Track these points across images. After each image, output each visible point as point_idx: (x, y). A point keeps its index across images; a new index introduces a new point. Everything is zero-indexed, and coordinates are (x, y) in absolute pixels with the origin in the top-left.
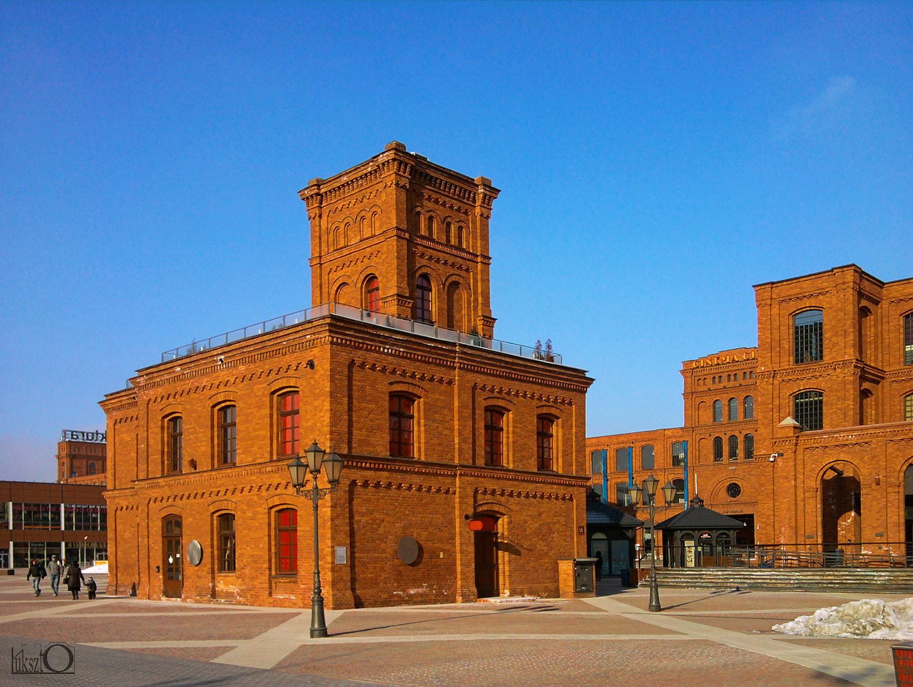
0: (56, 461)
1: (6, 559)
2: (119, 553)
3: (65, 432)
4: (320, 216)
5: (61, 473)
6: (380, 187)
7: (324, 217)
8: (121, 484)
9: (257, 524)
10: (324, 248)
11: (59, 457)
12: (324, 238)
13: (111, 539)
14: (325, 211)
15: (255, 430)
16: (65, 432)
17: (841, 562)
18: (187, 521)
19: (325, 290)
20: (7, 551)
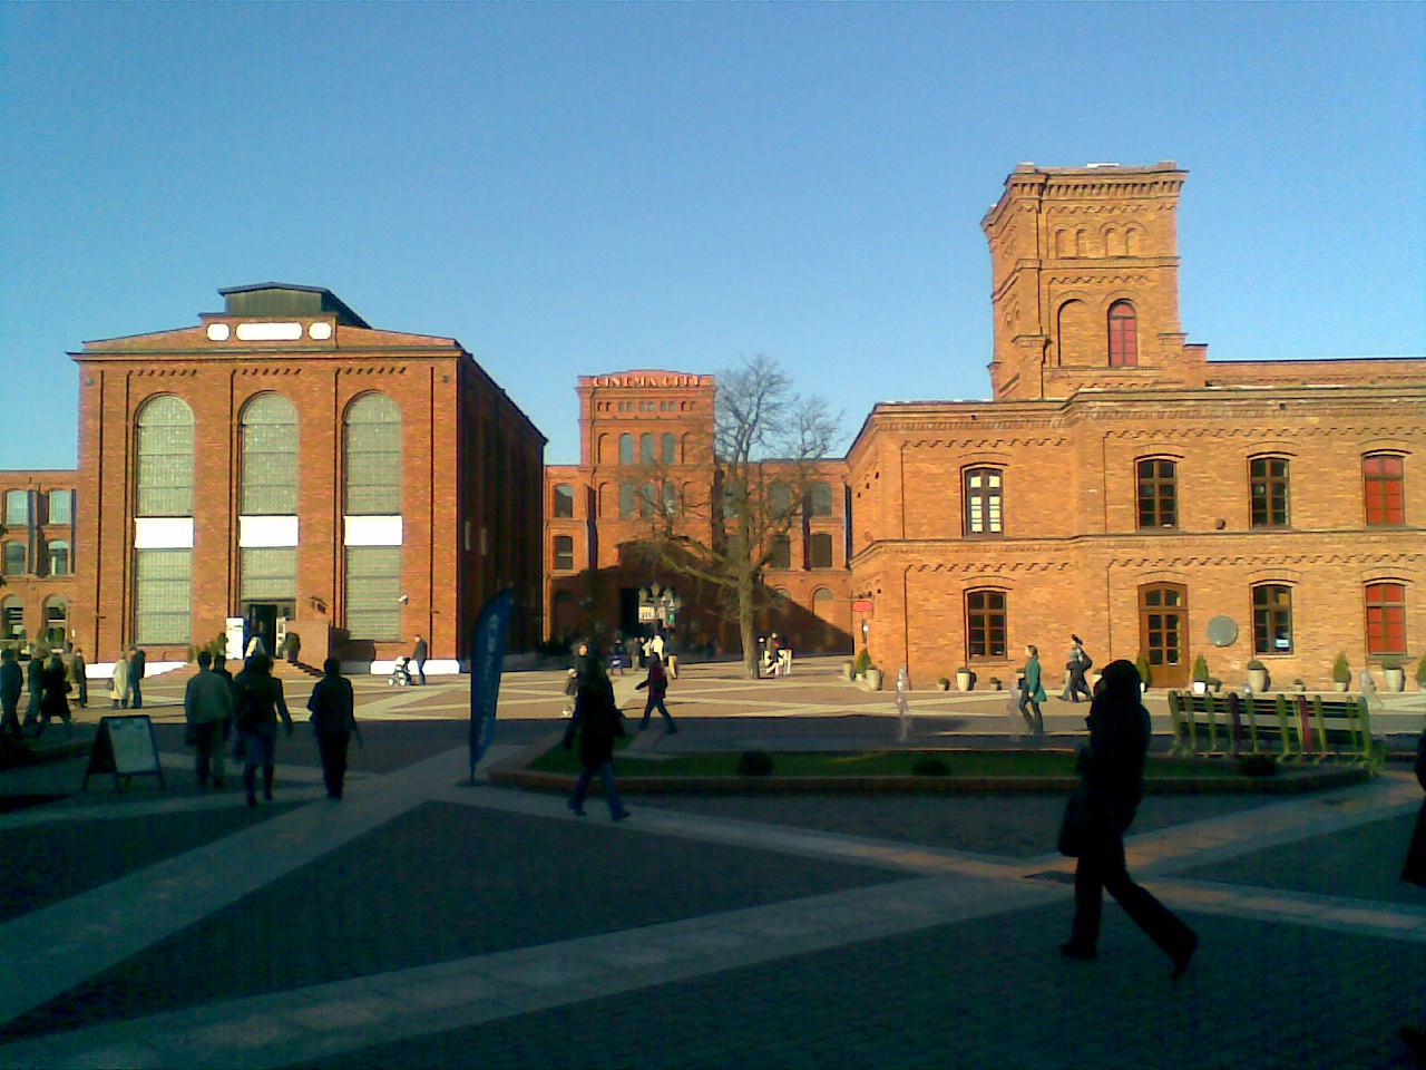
4: (1040, 211)
12: (1043, 237)
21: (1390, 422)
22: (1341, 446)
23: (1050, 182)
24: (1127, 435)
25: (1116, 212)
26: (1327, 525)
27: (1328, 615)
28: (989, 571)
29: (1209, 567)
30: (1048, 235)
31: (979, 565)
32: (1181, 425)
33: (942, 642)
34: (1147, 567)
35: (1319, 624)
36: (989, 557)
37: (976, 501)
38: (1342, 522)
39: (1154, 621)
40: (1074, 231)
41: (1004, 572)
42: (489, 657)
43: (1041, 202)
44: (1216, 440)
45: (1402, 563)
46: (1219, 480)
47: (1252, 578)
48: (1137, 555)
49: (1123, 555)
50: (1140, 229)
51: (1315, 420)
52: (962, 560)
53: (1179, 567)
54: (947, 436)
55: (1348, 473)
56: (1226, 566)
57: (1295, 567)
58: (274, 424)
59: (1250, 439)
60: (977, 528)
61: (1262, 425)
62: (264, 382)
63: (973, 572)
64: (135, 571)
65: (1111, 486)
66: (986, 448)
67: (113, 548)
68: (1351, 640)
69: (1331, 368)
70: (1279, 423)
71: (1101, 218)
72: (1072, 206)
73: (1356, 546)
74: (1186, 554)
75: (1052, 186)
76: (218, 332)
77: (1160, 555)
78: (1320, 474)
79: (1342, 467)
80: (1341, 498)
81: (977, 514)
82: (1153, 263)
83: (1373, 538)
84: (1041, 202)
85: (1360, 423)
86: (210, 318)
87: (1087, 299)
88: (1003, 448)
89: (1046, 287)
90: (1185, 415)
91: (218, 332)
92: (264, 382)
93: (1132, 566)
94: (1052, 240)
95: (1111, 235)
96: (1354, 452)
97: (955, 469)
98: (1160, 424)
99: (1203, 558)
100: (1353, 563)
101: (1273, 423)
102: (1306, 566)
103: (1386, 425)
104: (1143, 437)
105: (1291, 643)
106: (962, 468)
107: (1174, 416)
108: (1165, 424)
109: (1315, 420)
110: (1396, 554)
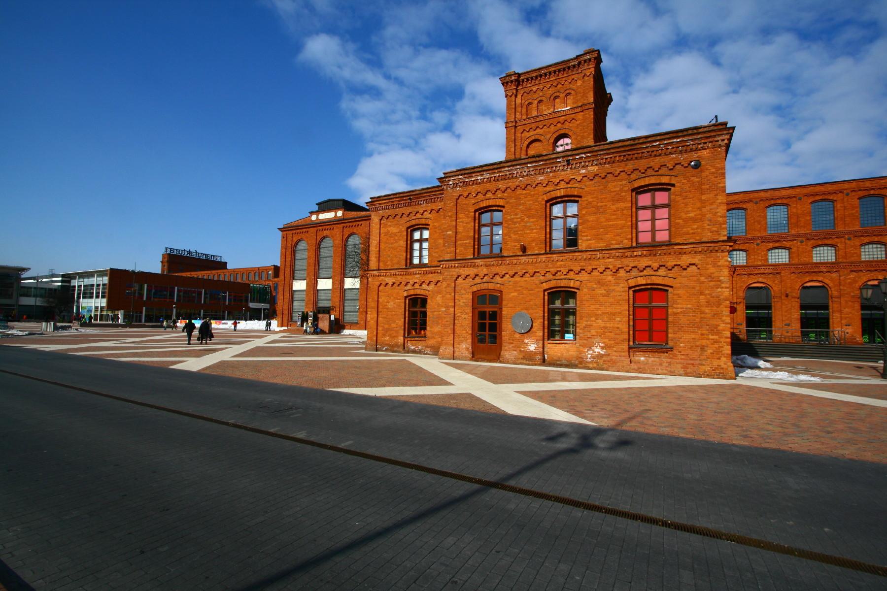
0: (160, 264)
1: (141, 317)
2: (380, 319)
3: (166, 248)
4: (516, 96)
5: (163, 270)
6: (575, 77)
7: (519, 96)
8: (385, 264)
9: (612, 300)
10: (518, 116)
11: (162, 262)
12: (519, 109)
13: (373, 308)
14: (521, 92)
15: (608, 220)
16: (166, 248)
17: (482, 341)
18: (510, 295)
19: (518, 144)
20: (141, 312)
21: (656, 162)
22: (614, 185)
23: (522, 78)
24: (471, 196)
25: (560, 86)
26: (602, 245)
27: (600, 312)
28: (417, 286)
29: (517, 278)
30: (522, 107)
31: (412, 283)
32: (501, 185)
33: (393, 325)
34: (478, 280)
35: (593, 319)
36: (416, 278)
37: (416, 246)
38: (614, 242)
39: (482, 315)
40: (536, 102)
41: (424, 286)
42: (239, 327)
43: (517, 91)
44: (524, 192)
45: (662, 272)
46: (526, 219)
47: (545, 286)
48: (472, 271)
49: (464, 272)
50: (573, 92)
51: (594, 169)
52: (403, 279)
53: (497, 279)
54: (399, 211)
55: (621, 205)
56: (527, 278)
57: (578, 278)
58: (329, 248)
59: (548, 189)
60: (416, 261)
61: (554, 177)
62: (325, 233)
63: (409, 287)
64: (292, 298)
65: (460, 229)
66: (419, 216)
67: (287, 289)
68: (618, 332)
69: (818, 188)
70: (568, 174)
71: (550, 92)
72: (534, 89)
73: (623, 260)
74: (502, 270)
75: (523, 80)
76: (314, 218)
77: (485, 271)
78: (598, 208)
79: (615, 201)
80: (613, 225)
81: (416, 253)
82: (579, 110)
83: (635, 253)
84: (517, 91)
85: (630, 166)
86: (312, 213)
87: (542, 138)
88: (427, 215)
89: (519, 135)
90: (504, 178)
91: (314, 218)
92: (325, 233)
93: (469, 280)
94: (524, 110)
95: (557, 100)
96: (626, 189)
97: (404, 229)
98: (489, 186)
99: (512, 273)
100: (622, 273)
101: (562, 175)
102: (584, 276)
103: (652, 164)
104: (480, 196)
105: (322, 332)
106: (408, 228)
107: (497, 180)
108: (492, 186)
109: (594, 169)
110: (655, 265)
